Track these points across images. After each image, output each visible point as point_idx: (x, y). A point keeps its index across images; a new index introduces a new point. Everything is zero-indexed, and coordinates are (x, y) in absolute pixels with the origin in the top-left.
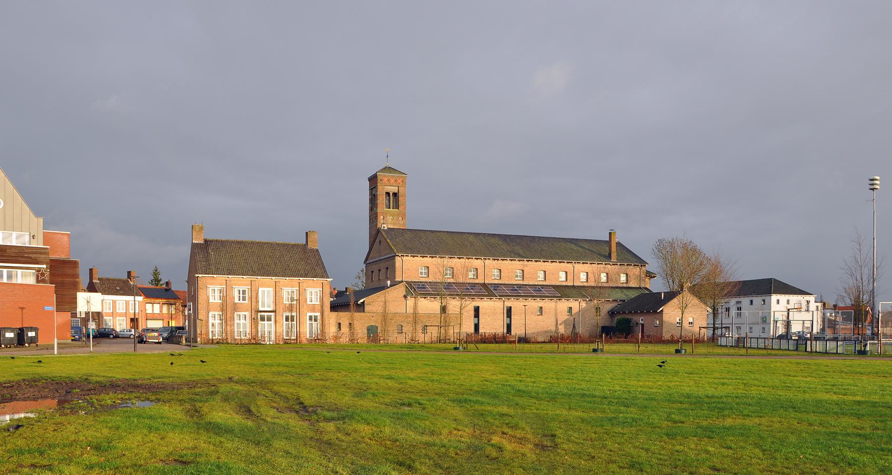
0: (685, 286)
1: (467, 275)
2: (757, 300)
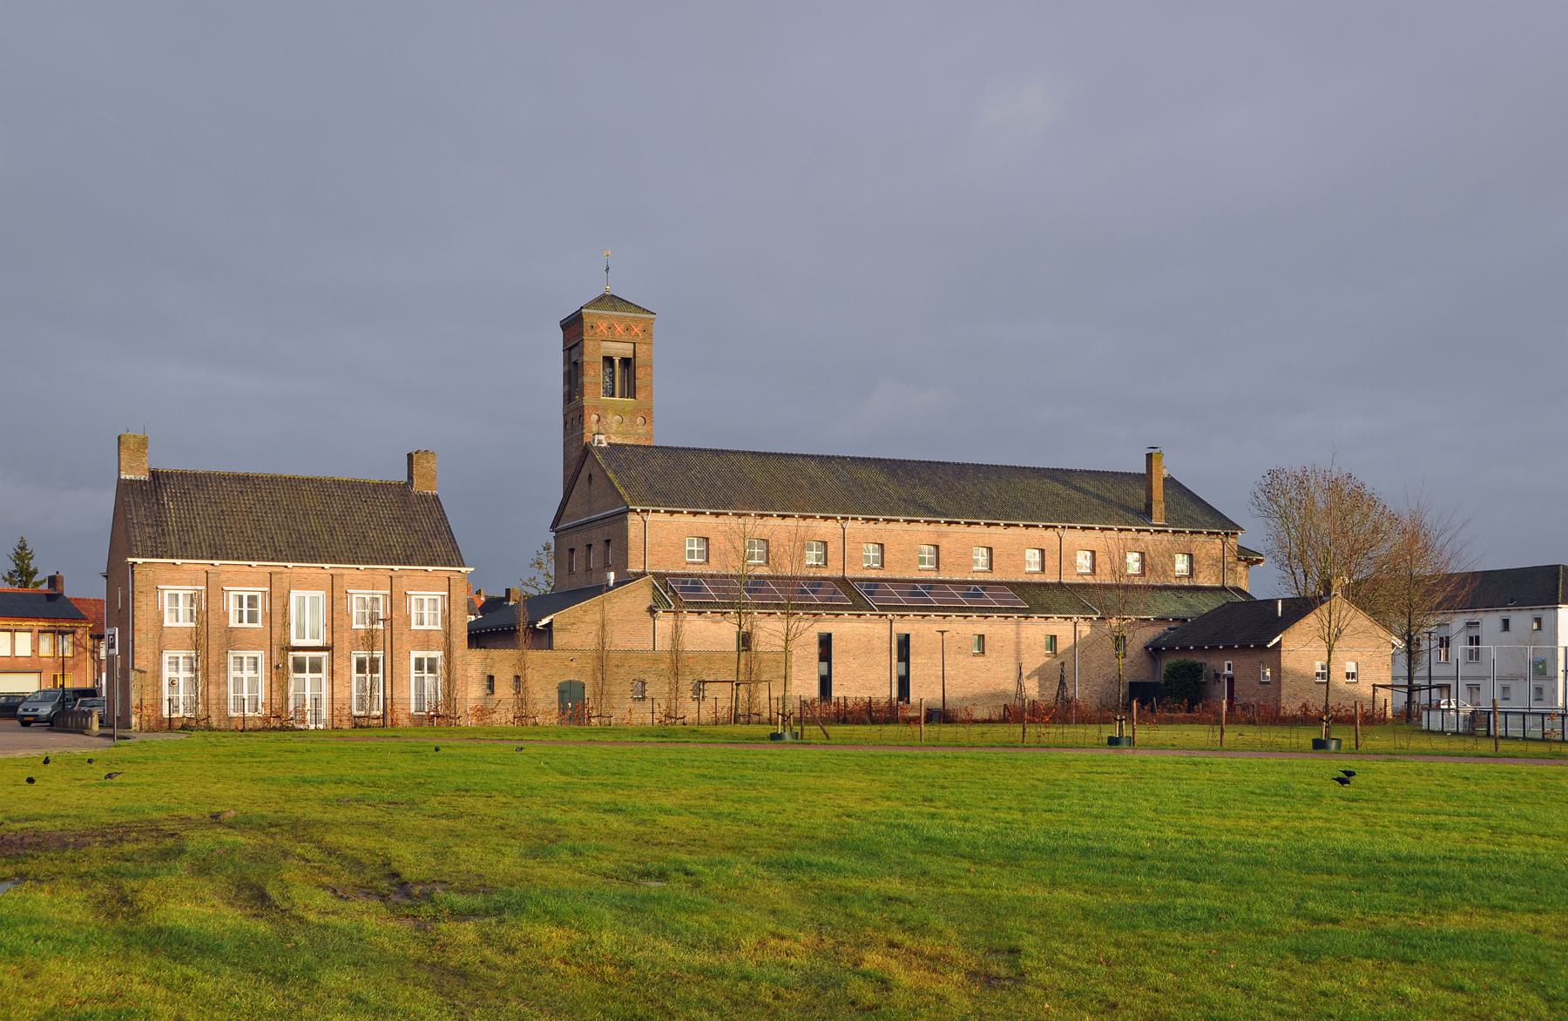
0: (1336, 584)
1: (802, 557)
2: (1522, 620)
